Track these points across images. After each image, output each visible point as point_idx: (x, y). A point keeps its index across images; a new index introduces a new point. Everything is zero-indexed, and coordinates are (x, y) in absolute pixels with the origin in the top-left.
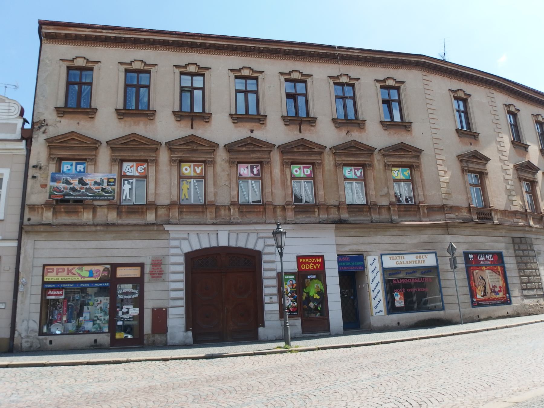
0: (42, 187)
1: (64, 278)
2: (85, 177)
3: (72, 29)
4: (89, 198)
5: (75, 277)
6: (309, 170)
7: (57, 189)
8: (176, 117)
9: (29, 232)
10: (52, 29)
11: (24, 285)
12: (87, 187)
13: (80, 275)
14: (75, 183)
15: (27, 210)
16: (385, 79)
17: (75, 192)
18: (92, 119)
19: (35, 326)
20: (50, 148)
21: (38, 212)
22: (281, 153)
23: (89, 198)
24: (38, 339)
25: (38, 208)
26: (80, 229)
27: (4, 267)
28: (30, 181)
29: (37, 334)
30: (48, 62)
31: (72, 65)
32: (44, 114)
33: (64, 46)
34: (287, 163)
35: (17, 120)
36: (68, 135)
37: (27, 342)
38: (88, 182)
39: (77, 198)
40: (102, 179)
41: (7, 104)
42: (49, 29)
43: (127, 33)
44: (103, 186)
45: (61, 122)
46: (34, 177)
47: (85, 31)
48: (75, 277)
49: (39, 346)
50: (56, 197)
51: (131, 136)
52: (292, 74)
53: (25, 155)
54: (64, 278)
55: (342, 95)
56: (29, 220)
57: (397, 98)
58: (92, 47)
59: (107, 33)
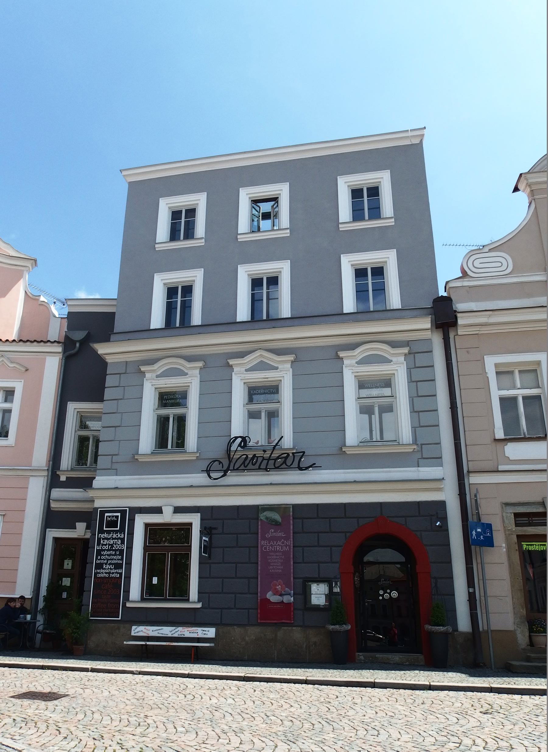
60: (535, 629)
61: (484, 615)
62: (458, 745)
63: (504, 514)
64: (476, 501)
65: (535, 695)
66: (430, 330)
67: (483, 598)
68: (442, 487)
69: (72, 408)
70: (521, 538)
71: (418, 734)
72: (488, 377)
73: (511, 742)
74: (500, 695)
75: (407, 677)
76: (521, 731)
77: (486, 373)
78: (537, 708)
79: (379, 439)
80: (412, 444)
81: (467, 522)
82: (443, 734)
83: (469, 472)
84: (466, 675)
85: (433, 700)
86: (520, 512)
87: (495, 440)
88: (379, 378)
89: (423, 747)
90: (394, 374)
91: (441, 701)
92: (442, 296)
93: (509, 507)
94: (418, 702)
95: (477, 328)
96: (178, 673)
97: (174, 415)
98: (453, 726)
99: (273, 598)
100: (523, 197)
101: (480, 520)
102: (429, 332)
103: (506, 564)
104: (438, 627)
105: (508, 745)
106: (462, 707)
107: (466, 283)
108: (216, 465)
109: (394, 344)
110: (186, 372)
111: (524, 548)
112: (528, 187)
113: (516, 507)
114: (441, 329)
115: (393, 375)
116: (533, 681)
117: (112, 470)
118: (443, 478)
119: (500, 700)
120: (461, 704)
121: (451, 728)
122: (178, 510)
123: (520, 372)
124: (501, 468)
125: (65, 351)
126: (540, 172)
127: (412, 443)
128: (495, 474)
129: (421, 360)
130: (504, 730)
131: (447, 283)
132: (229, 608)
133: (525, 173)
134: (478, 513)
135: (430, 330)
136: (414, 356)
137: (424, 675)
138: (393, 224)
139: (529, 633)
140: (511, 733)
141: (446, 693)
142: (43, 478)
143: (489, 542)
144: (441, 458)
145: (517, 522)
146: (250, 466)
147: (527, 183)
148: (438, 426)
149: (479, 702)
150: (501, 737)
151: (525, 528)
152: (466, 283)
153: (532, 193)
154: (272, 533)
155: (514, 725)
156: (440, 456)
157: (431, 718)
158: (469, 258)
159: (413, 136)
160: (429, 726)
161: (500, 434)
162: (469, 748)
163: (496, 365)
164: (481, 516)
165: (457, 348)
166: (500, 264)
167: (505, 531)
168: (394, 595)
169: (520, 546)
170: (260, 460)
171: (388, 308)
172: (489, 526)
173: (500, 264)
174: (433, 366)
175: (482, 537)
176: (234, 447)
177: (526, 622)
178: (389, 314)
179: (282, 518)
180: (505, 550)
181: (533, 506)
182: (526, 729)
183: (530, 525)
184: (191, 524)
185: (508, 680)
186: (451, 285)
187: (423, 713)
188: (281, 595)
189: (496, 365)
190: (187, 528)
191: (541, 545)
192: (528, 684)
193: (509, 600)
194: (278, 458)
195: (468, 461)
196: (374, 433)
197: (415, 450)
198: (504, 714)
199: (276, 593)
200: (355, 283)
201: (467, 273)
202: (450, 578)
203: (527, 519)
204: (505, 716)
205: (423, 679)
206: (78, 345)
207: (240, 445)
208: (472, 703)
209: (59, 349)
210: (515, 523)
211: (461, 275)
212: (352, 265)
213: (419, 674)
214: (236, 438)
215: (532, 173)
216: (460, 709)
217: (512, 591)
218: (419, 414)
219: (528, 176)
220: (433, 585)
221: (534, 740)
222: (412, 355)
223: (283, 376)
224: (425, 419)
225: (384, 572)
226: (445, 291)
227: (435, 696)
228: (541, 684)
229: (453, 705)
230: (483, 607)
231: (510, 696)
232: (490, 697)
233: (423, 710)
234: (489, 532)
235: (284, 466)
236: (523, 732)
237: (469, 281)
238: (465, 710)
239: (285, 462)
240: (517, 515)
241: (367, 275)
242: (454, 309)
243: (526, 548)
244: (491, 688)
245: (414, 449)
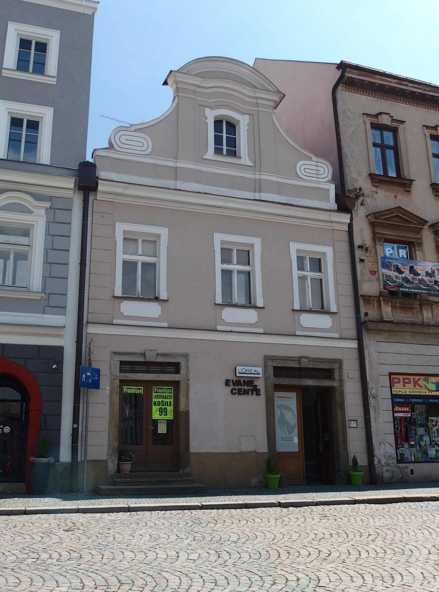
0: (371, 274)
1: (412, 390)
2: (416, 265)
3: (378, 77)
4: (424, 292)
5: (423, 390)
6: (405, 251)
7: (388, 278)
8: (435, 191)
9: (371, 330)
10: (357, 74)
11: (374, 398)
12: (420, 277)
13: (427, 388)
14: (407, 273)
15: (361, 303)
16: (436, 126)
17: (408, 284)
18: (408, 193)
19: (391, 450)
20: (373, 225)
21: (373, 305)
22: (370, 224)
23: (424, 292)
24: (399, 467)
25: (373, 300)
26: (425, 330)
27: (348, 374)
28: (359, 266)
29: (395, 461)
30: (351, 115)
31: (376, 122)
32: (357, 180)
33: (363, 96)
34: (380, 240)
35: (329, 185)
36: (394, 210)
37: (388, 471)
38: (419, 272)
39: (412, 291)
40: (433, 269)
41: (314, 163)
42: (353, 73)
43: (433, 90)
44: (435, 279)
45: (377, 193)
46: (362, 261)
47: (391, 82)
48: (423, 390)
49: (401, 476)
50: (391, 288)
51: (394, 210)
52: (379, 117)
53: (347, 231)
54: (412, 390)
55: (206, 108)
56: (366, 314)
57: (392, 143)
58: (391, 102)
59: (412, 87)
60: (123, 459)
61: (83, 447)
62: (35, 560)
63: (112, 361)
64: (90, 348)
65: (113, 512)
66: (72, 190)
67: (84, 433)
68: (62, 334)
70: (123, 382)
71: (3, 554)
72: (116, 241)
73: (81, 553)
74: (85, 514)
75: (6, 505)
76: (93, 543)
77: (115, 237)
78: (111, 523)
79: (10, 284)
80: (41, 292)
81: (80, 367)
82: (25, 552)
83: (88, 322)
84: (60, 499)
85: (24, 523)
86: (125, 360)
87: (114, 297)
88: (18, 227)
89: (3, 565)
90: (33, 225)
91: (32, 524)
92: (88, 161)
93: (117, 355)
94: (11, 526)
95: (113, 197)
96: (44, 510)
98: (36, 544)
100: (169, 91)
101: (91, 366)
102: (71, 191)
103: (108, 404)
104: (41, 459)
105: (79, 555)
106: (49, 527)
107: (111, 154)
109: (37, 197)
110: (32, 210)
111: (125, 390)
112: (175, 84)
113: (122, 356)
114: (83, 191)
115: (32, 226)
116: (114, 501)
118: (64, 326)
119: (83, 519)
120: (49, 525)
121: (34, 546)
123: (143, 241)
124: (115, 321)
126: (186, 74)
127: (40, 291)
128: (213, 333)
129: (60, 216)
130: (79, 544)
131: (95, 150)
133: (175, 71)
134: (90, 359)
135: (72, 190)
136: (55, 211)
137: (22, 501)
138: (55, 83)
139: (118, 462)
140: (84, 546)
141: (38, 516)
143: (96, 385)
144: (65, 307)
145: (122, 369)
147: (175, 81)
148: (67, 278)
149: (65, 522)
150: (74, 550)
151: (127, 374)
152: (111, 154)
153: (177, 90)
155: (89, 538)
156: (65, 306)
157: (19, 539)
158: (116, 134)
159: (87, 6)
160: (15, 546)
161: (118, 292)
162: (44, 562)
163: (125, 232)
164: (92, 362)
165: (94, 210)
166: (306, 170)
167: (111, 375)
168: (6, 431)
169: (121, 389)
171: (37, 162)
172: (98, 371)
173: (306, 170)
174: (70, 224)
175: (90, 380)
177: (117, 454)
178: (38, 168)
180: (108, 392)
181: (136, 356)
182: (97, 541)
183: (163, 372)
185: (94, 502)
186: (98, 153)
187: (12, 535)
189: (125, 232)
191: (168, 389)
192: (110, 503)
193: (105, 435)
195: (88, 313)
196: (7, 277)
197: (43, 298)
198: (83, 530)
200: (9, 131)
201: (113, 146)
202: (59, 415)
203: (130, 366)
204: (84, 531)
205: (21, 505)
208: (59, 523)
210: (120, 370)
211: (108, 146)
212: (9, 113)
213: (18, 501)
215: (180, 72)
216: (46, 529)
217: (109, 427)
218: (51, 265)
219: (177, 74)
220: (43, 421)
221: (101, 549)
222: (53, 210)
223: (36, 220)
224: (57, 271)
225: (8, 409)
226: (92, 158)
227: (28, 519)
228: (119, 503)
229: (41, 526)
230: (83, 441)
231: (93, 514)
232: (75, 517)
233: (13, 532)
234: (97, 376)
236: (94, 544)
237: (114, 153)
238: (50, 530)
240: (122, 363)
241: (22, 126)
242: (97, 175)
243: (126, 391)
244: (79, 509)
245: (42, 297)
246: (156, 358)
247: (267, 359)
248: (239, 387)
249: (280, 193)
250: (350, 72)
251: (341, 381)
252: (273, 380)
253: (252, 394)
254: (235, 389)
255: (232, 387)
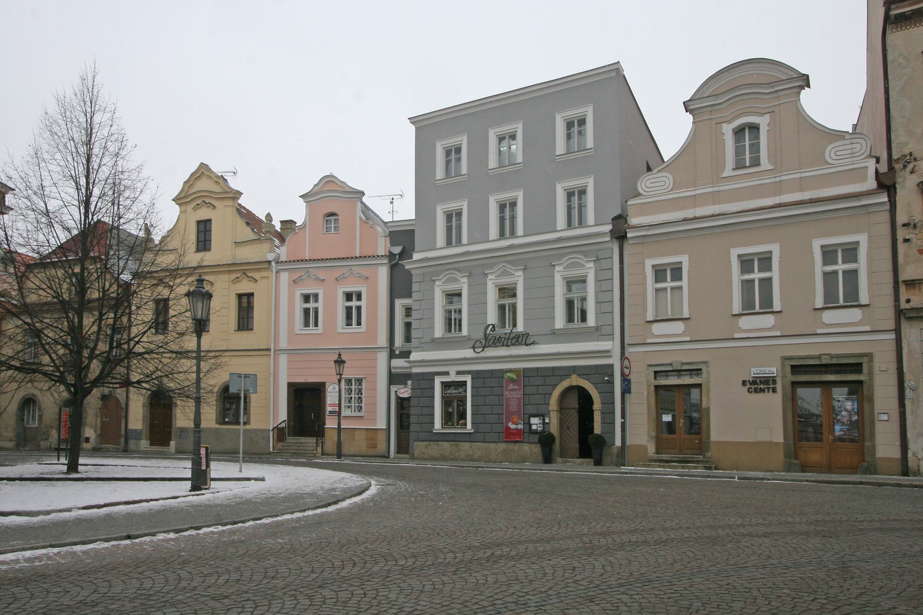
11: (913, 390)
28: (901, 247)
42: (902, 7)
46: (906, 241)
69: (399, 303)
97: (509, 304)
99: (512, 426)
108: (478, 344)
117: (420, 348)
122: (458, 373)
124: (649, 341)
125: (390, 262)
132: (489, 432)
142: (386, 350)
146: (498, 344)
154: (511, 386)
170: (503, 339)
176: (488, 331)
179: (517, 377)
184: (466, 382)
188: (517, 424)
190: (464, 384)
194: (514, 338)
199: (514, 423)
206: (397, 257)
207: (491, 330)
209: (386, 261)
214: (489, 325)
235: (517, 343)
239: (517, 341)
246: (681, 366)
247: (785, 358)
248: (756, 386)
249: (802, 190)
250: (897, 8)
251: (871, 374)
252: (790, 378)
253: (768, 392)
254: (751, 388)
255: (749, 386)
